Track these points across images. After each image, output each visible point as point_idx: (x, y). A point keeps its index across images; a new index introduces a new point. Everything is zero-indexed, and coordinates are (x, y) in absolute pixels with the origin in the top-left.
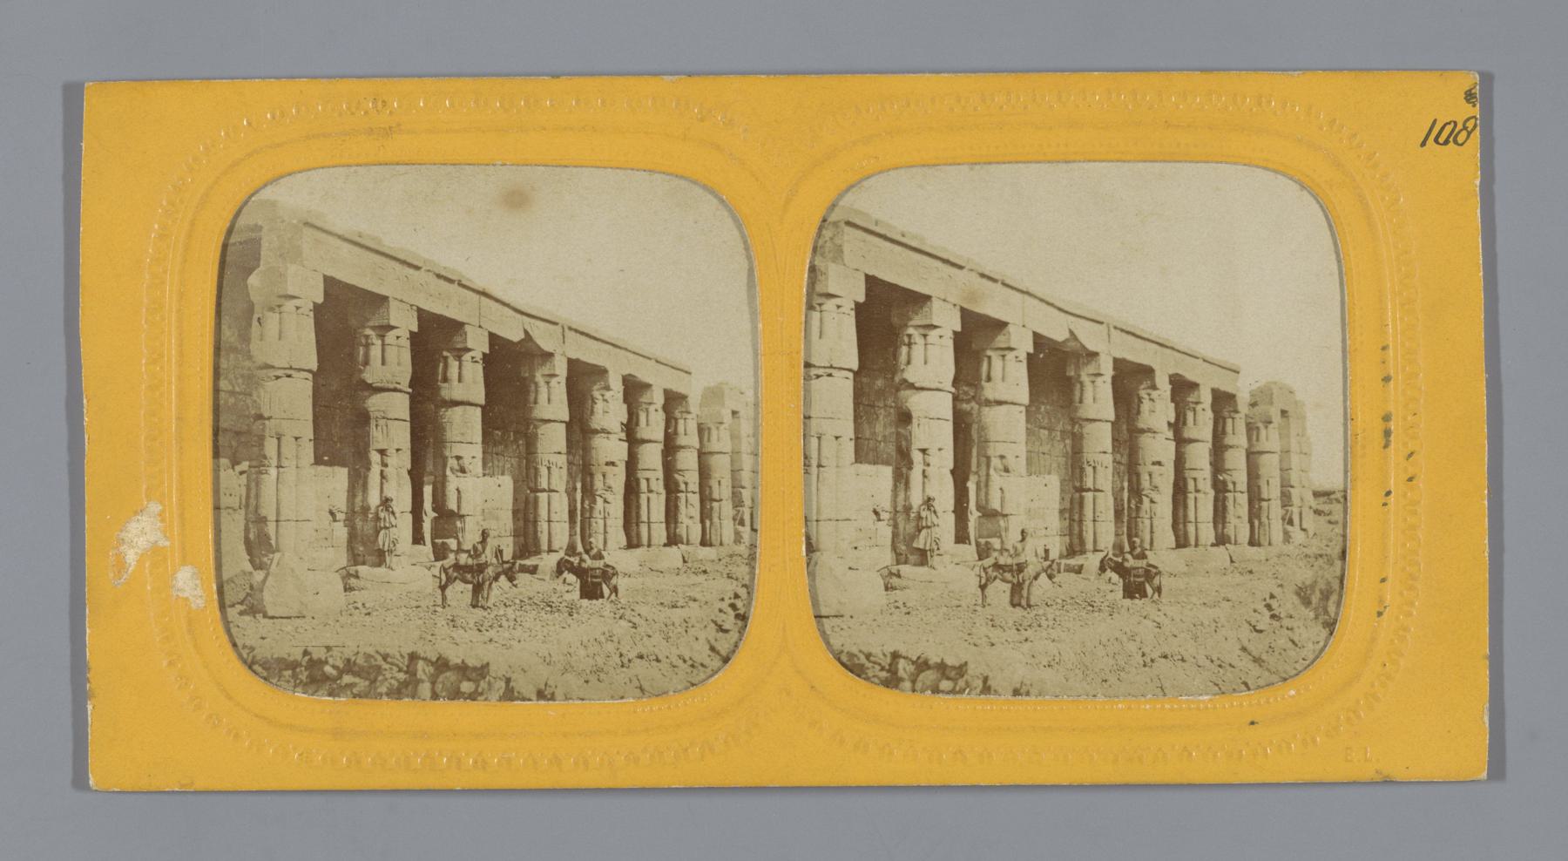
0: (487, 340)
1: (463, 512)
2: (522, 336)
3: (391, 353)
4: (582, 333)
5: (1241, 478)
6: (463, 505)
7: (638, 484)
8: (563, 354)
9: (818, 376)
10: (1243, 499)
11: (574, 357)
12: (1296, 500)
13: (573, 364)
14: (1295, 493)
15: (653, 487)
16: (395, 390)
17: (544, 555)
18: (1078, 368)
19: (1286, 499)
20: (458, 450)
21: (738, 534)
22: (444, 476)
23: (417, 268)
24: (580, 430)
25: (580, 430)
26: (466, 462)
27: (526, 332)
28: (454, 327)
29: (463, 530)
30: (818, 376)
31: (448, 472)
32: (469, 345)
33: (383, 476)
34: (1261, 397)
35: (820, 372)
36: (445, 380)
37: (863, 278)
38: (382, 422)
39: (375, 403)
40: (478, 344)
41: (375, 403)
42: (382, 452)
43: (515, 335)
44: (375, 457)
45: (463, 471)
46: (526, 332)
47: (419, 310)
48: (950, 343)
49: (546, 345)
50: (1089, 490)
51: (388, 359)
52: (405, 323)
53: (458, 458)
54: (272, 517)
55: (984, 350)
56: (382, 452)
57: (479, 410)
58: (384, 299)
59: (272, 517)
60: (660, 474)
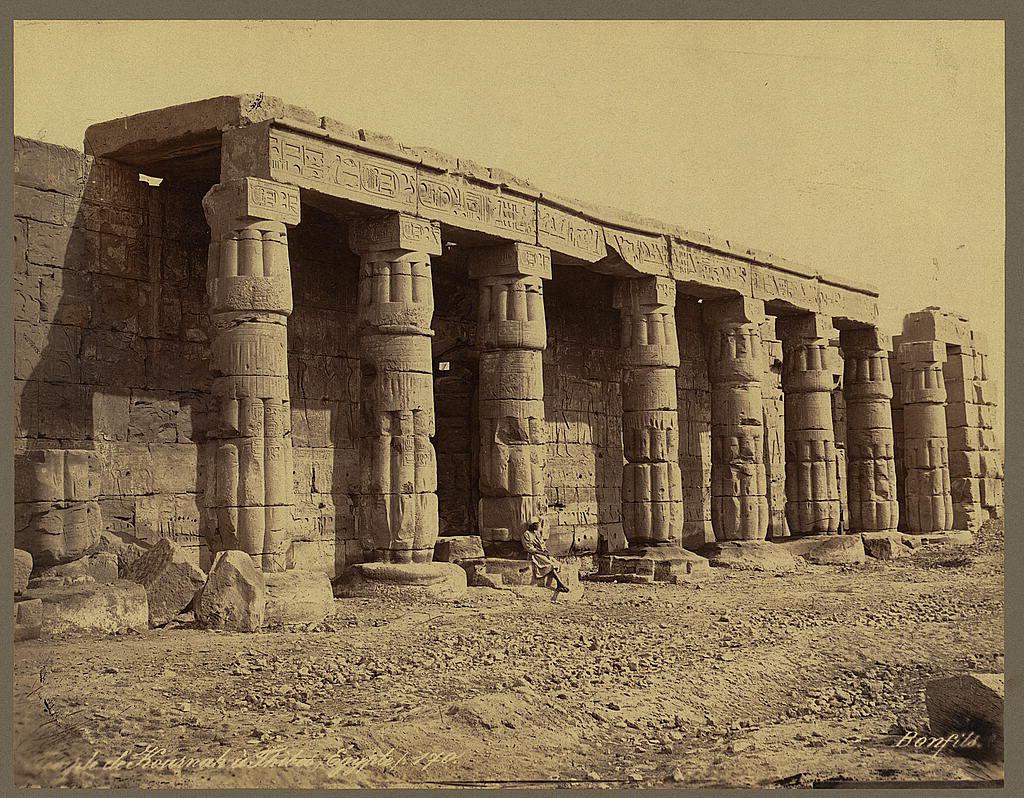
10: (889, 468)
14: (973, 459)
33: (397, 447)
44: (386, 423)
49: (642, 267)
50: (646, 460)
58: (394, 214)
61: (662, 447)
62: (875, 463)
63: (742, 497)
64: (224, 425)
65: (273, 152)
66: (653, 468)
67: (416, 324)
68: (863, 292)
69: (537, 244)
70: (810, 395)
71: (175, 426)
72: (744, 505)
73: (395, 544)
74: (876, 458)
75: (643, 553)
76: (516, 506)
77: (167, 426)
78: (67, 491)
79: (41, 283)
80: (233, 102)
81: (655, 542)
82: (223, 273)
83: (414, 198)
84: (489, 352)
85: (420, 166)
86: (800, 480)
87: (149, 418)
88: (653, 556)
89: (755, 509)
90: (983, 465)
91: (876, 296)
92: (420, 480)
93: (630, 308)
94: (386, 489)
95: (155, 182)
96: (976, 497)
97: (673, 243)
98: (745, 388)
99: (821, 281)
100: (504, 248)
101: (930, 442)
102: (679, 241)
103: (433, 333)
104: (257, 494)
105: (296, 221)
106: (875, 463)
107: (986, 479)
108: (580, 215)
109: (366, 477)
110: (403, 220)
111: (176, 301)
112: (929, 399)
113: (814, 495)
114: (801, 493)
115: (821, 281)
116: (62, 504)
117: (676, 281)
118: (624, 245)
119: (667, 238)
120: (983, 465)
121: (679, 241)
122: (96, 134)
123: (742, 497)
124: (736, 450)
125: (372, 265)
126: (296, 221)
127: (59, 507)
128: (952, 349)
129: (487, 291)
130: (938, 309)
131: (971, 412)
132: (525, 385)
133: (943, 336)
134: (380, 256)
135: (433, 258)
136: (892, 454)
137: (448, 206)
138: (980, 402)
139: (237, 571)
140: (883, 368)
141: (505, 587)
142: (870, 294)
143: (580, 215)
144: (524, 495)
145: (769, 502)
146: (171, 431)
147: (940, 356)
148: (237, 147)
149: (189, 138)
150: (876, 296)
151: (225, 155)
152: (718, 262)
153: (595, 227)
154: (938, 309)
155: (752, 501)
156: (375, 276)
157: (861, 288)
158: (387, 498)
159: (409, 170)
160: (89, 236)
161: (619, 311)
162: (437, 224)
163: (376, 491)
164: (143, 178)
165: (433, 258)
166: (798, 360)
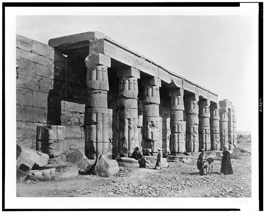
0: (161, 82)
1: (154, 140)
2: (171, 82)
3: (132, 86)
4: (188, 82)
5: (218, 129)
6: (154, 137)
7: (202, 131)
8: (183, 88)
9: (96, 93)
10: (218, 136)
11: (186, 89)
12: (232, 136)
13: (185, 91)
14: (232, 134)
15: (207, 132)
16: (133, 98)
17: (177, 154)
18: (172, 93)
19: (229, 136)
20: (152, 119)
21: (230, 146)
22: (147, 128)
23: (140, 57)
24: (187, 114)
25: (187, 114)
26: (155, 123)
27: (172, 80)
28: (151, 78)
29: (153, 145)
30: (96, 93)
31: (148, 126)
32: (155, 84)
33: (129, 128)
34: (223, 103)
35: (96, 91)
36: (148, 95)
37: (110, 59)
38: (129, 109)
39: (127, 102)
40: (158, 84)
41: (127, 102)
42: (129, 119)
43: (169, 82)
44: (127, 121)
45: (153, 126)
46: (172, 80)
47: (140, 71)
48: (137, 82)
49: (178, 85)
50: (176, 133)
51: (131, 88)
52: (136, 76)
53: (152, 122)
54: (95, 141)
55: (145, 86)
56: (129, 119)
57: (158, 106)
58: (130, 67)
59: (95, 141)
60: (209, 128)
61: (180, 129)
62: (216, 135)
63: (194, 142)
64: (92, 120)
65: (105, 47)
66: (178, 135)
67: (134, 96)
68: (215, 95)
69: (158, 78)
70: (205, 118)
71: (70, 121)
72: (194, 144)
73: (129, 152)
74: (216, 133)
75: (175, 155)
76: (153, 143)
77: (69, 121)
78: (57, 137)
79: (39, 81)
80: (92, 33)
81: (178, 153)
82: (92, 79)
83: (135, 64)
84: (147, 105)
85: (136, 55)
86: (202, 138)
87: (65, 118)
88: (178, 156)
89: (196, 145)
90: (234, 136)
91: (217, 96)
92: (135, 136)
93: (173, 96)
94: (127, 138)
95: (66, 56)
96: (232, 143)
97: (184, 80)
98: (195, 116)
99: (209, 92)
100: (152, 78)
101: (224, 130)
102: (185, 80)
103: (138, 99)
104: (100, 139)
105: (110, 66)
106: (216, 135)
107: (234, 139)
108: (167, 71)
109: (121, 135)
110: (132, 69)
111: (71, 88)
112: (224, 121)
113: (206, 142)
114: (202, 141)
115: (209, 92)
116: (56, 141)
117: (184, 90)
118: (175, 80)
119: (182, 79)
120: (234, 136)
121: (185, 80)
122: (51, 42)
123: (194, 142)
124: (192, 131)
125: (123, 80)
126: (110, 66)
127: (55, 142)
128: (229, 109)
129: (146, 89)
130: (227, 100)
131: (232, 123)
132: (156, 113)
133: (228, 106)
134: (125, 78)
135: (138, 79)
136: (219, 133)
137: (141, 66)
138: (234, 121)
139: (105, 160)
140: (218, 113)
141: (151, 163)
142: (216, 96)
143: (167, 71)
144: (155, 141)
145: (178, 144)
146: (70, 122)
147: (227, 111)
148: (94, 45)
149: (80, 43)
150: (217, 96)
151: (90, 48)
152: (191, 85)
153: (170, 75)
154: (227, 100)
155: (195, 143)
156: (124, 83)
157: (215, 94)
158: (127, 141)
159: (133, 55)
160: (51, 69)
161: (170, 96)
162: (139, 71)
163: (124, 139)
164: (63, 55)
165: (138, 79)
166: (202, 110)
